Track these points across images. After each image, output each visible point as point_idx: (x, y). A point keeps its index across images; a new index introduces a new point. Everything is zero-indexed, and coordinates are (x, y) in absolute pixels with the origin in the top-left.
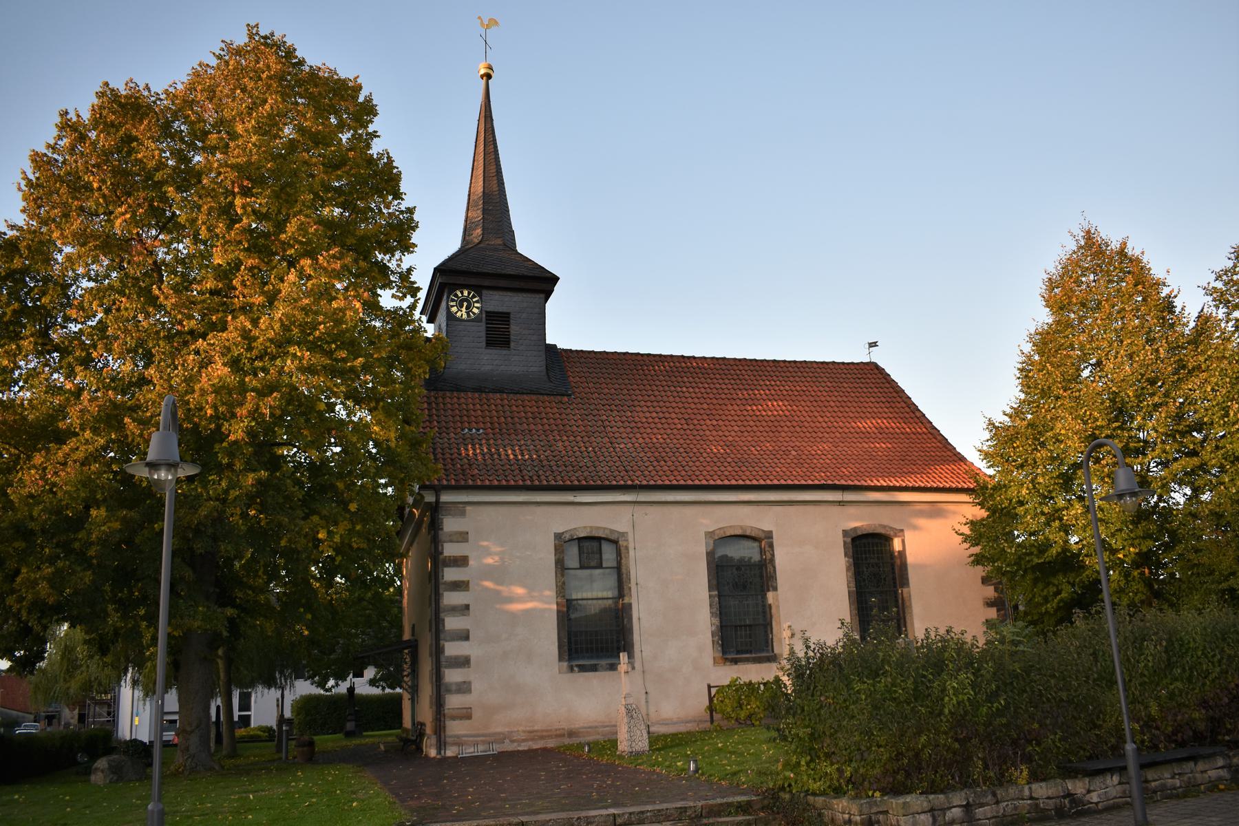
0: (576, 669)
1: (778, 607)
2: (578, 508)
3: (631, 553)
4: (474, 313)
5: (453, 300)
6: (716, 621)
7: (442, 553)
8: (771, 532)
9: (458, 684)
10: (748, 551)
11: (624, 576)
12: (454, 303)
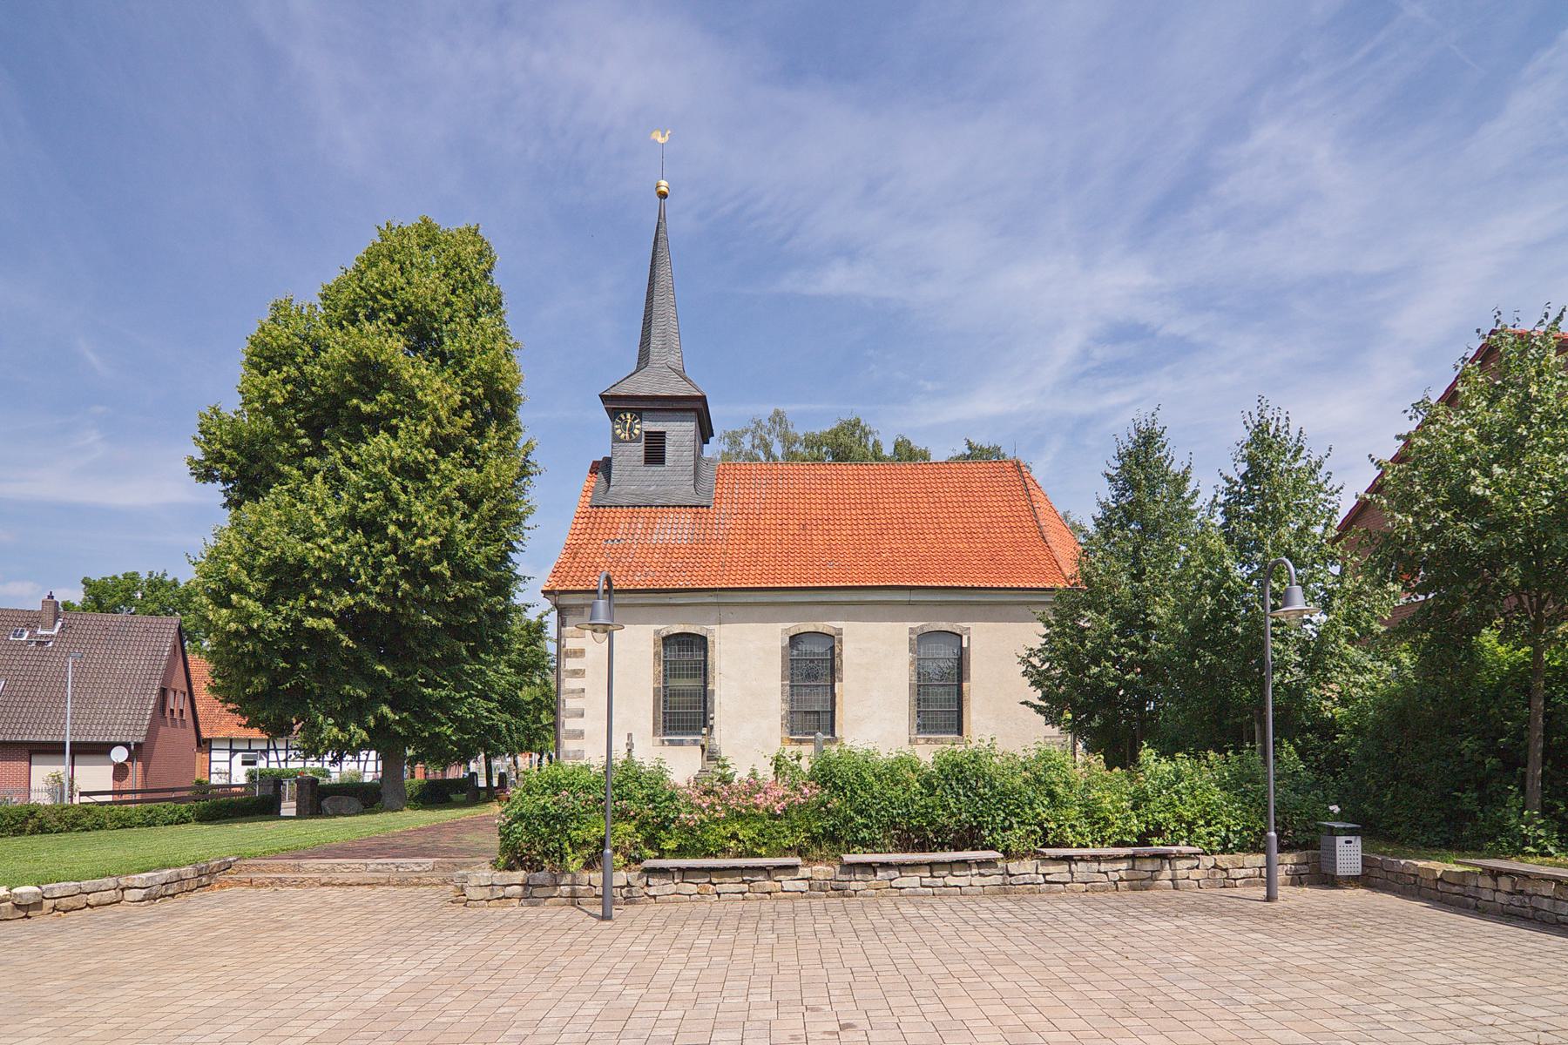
2: (679, 608)
3: (717, 646)
5: (618, 423)
6: (786, 707)
7: (564, 646)
9: (575, 752)
10: (819, 649)
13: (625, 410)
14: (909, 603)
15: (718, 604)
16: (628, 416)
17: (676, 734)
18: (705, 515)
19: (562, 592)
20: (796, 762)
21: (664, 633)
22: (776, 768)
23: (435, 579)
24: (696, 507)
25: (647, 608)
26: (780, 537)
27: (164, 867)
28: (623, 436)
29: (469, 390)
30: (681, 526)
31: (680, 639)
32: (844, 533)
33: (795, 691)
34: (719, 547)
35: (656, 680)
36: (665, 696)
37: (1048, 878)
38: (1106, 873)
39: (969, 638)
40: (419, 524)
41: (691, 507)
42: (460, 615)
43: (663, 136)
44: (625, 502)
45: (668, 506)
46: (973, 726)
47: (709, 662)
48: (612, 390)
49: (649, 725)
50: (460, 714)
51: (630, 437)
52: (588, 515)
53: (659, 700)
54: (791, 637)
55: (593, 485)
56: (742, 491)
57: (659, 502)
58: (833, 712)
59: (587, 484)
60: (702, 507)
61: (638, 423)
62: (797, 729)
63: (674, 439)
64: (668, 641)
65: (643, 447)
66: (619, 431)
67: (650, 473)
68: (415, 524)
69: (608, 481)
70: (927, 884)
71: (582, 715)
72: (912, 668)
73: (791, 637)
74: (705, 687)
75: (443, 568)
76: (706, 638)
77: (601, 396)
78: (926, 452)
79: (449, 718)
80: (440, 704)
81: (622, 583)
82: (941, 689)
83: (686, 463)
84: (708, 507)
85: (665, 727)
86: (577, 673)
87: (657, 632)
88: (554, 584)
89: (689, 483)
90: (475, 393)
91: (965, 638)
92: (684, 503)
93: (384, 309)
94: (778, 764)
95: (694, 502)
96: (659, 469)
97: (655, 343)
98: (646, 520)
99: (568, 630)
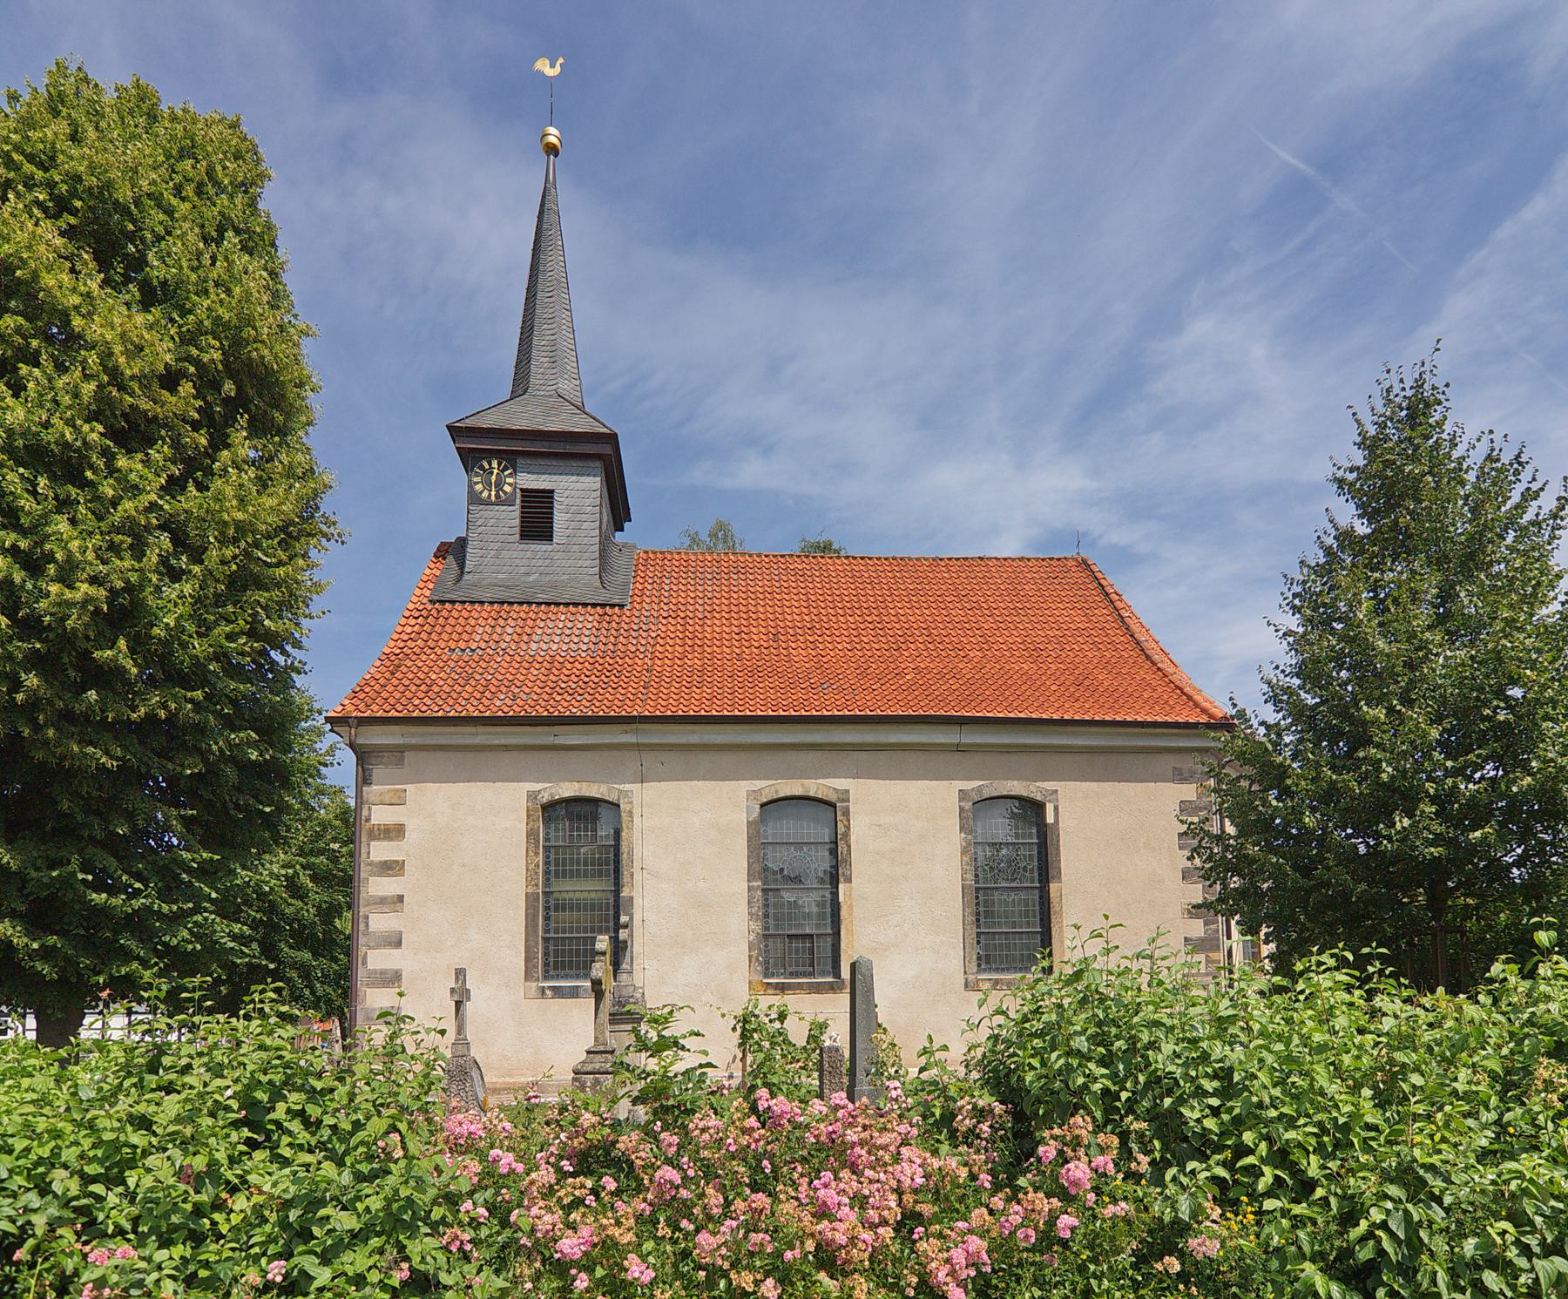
0: (548, 993)
1: (851, 907)
3: (637, 820)
4: (505, 493)
5: (477, 475)
6: (757, 927)
7: (368, 820)
8: (847, 791)
11: (625, 856)
12: (479, 479)
14: (959, 749)
15: (638, 747)
16: (495, 464)
17: (566, 977)
19: (363, 721)
20: (777, 1025)
21: (545, 798)
22: (743, 1036)
23: (107, 677)
24: (603, 605)
25: (515, 754)
26: (737, 651)
27: (665, 1006)
28: (485, 494)
29: (195, 352)
30: (577, 632)
31: (577, 808)
32: (840, 647)
33: (771, 900)
34: (640, 662)
35: (531, 878)
36: (547, 909)
39: (1056, 808)
40: (59, 556)
41: (594, 605)
42: (170, 760)
43: (552, 66)
44: (487, 595)
45: (557, 604)
47: (624, 848)
48: (467, 421)
49: (515, 960)
50: (174, 942)
51: (497, 496)
52: (424, 613)
53: (535, 916)
54: (762, 806)
55: (438, 573)
56: (675, 588)
57: (542, 597)
58: (837, 934)
59: (428, 571)
60: (612, 606)
61: (510, 475)
62: (775, 965)
63: (567, 501)
64: (552, 810)
65: (517, 514)
66: (479, 487)
67: (529, 554)
68: (50, 557)
69: (462, 566)
71: (398, 944)
73: (762, 806)
74: (617, 892)
75: (118, 653)
77: (449, 427)
79: (155, 950)
80: (138, 923)
81: (472, 709)
82: (1013, 896)
83: (586, 540)
84: (621, 606)
85: (546, 965)
86: (391, 868)
87: (532, 796)
88: (350, 708)
89: (591, 571)
90: (206, 358)
91: (1050, 808)
92: (583, 600)
93: (30, 184)
94: (747, 1028)
95: (600, 599)
96: (544, 548)
97: (539, 361)
98: (521, 623)
99: (373, 791)
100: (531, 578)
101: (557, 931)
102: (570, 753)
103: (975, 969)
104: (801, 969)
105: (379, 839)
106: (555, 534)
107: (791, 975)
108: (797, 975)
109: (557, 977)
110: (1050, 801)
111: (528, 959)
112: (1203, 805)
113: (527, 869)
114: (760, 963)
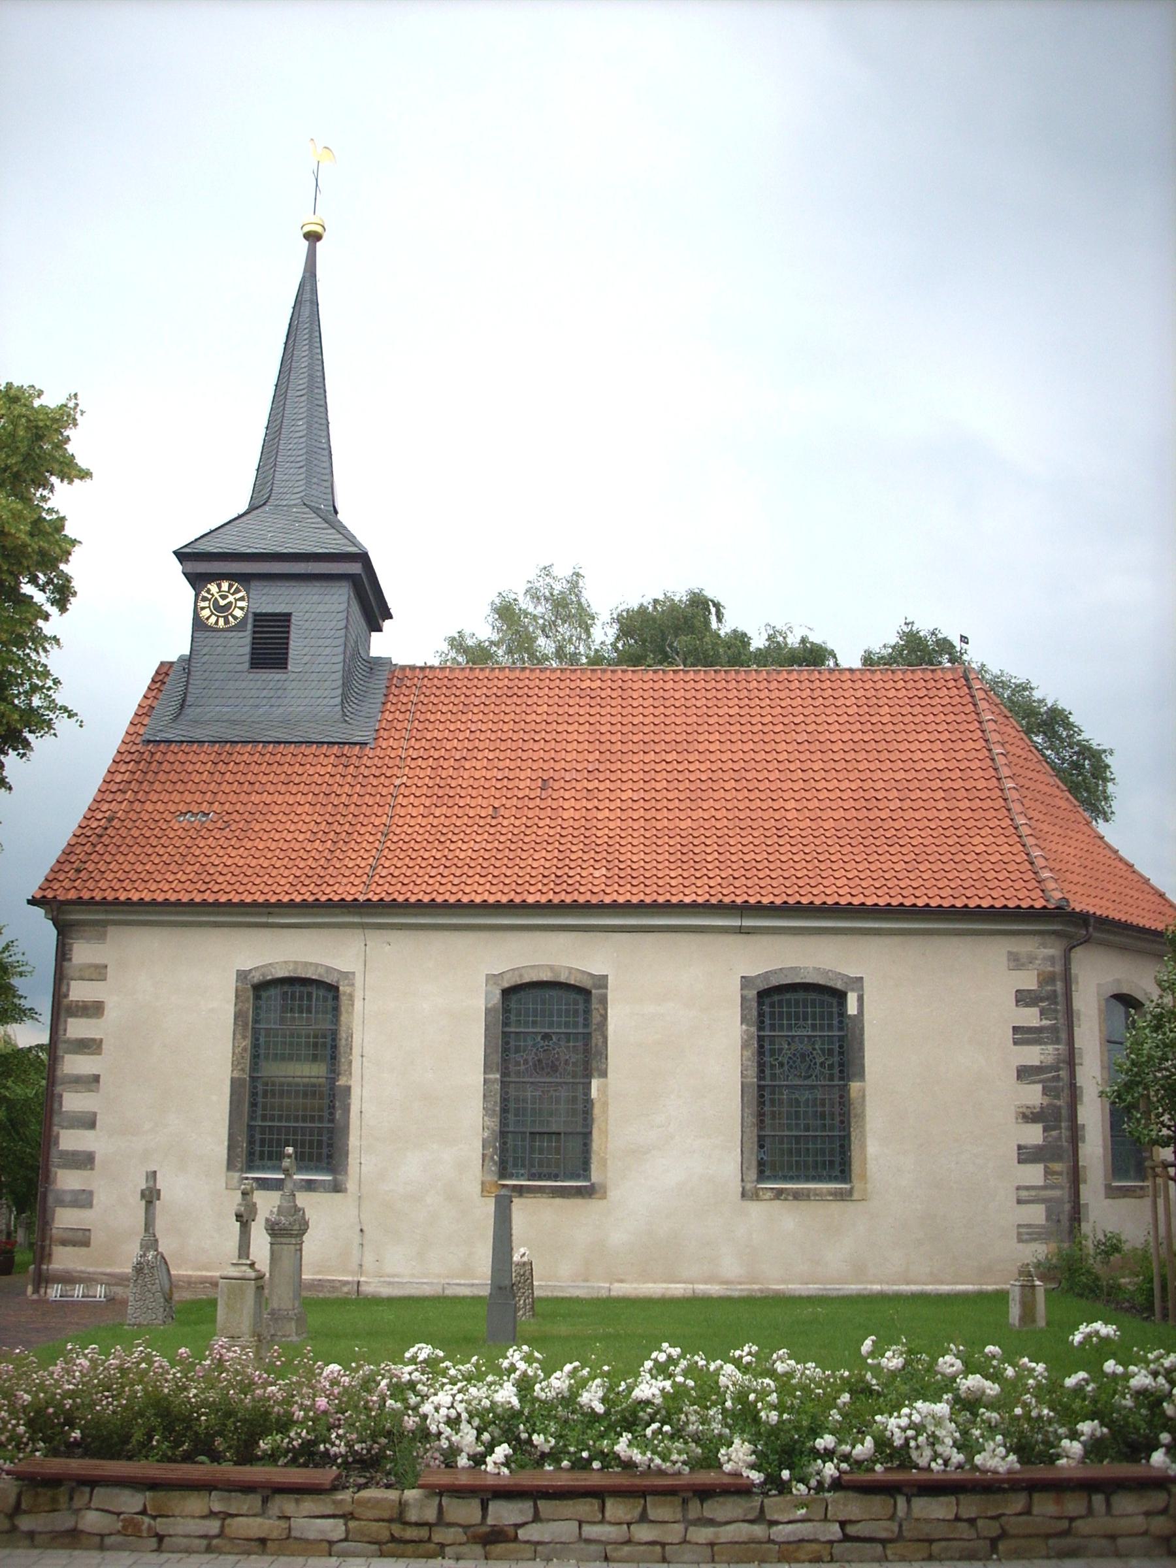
1: (605, 1104)
3: (358, 1004)
4: (235, 618)
7: (67, 996)
13: (217, 577)
18: (354, 760)
37: (852, 1530)
38: (972, 1521)
39: (861, 999)
46: (872, 1167)
48: (197, 545)
65: (248, 640)
70: (593, 1536)
72: (748, 1053)
76: (337, 989)
77: (175, 553)
78: (793, 656)
92: (319, 738)
96: (278, 677)
100: (261, 711)
101: (264, 1118)
102: (285, 930)
103: (755, 1177)
104: (545, 1170)
105: (76, 1016)
106: (290, 662)
107: (532, 1177)
108: (540, 1177)
109: (263, 1169)
110: (853, 990)
111: (231, 1148)
112: (1044, 994)
113: (234, 1053)
114: (495, 1163)
